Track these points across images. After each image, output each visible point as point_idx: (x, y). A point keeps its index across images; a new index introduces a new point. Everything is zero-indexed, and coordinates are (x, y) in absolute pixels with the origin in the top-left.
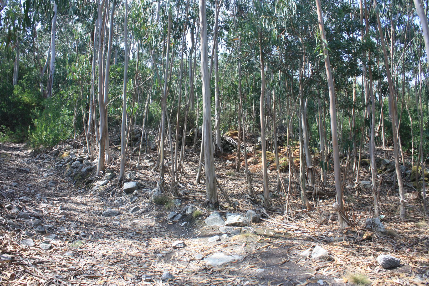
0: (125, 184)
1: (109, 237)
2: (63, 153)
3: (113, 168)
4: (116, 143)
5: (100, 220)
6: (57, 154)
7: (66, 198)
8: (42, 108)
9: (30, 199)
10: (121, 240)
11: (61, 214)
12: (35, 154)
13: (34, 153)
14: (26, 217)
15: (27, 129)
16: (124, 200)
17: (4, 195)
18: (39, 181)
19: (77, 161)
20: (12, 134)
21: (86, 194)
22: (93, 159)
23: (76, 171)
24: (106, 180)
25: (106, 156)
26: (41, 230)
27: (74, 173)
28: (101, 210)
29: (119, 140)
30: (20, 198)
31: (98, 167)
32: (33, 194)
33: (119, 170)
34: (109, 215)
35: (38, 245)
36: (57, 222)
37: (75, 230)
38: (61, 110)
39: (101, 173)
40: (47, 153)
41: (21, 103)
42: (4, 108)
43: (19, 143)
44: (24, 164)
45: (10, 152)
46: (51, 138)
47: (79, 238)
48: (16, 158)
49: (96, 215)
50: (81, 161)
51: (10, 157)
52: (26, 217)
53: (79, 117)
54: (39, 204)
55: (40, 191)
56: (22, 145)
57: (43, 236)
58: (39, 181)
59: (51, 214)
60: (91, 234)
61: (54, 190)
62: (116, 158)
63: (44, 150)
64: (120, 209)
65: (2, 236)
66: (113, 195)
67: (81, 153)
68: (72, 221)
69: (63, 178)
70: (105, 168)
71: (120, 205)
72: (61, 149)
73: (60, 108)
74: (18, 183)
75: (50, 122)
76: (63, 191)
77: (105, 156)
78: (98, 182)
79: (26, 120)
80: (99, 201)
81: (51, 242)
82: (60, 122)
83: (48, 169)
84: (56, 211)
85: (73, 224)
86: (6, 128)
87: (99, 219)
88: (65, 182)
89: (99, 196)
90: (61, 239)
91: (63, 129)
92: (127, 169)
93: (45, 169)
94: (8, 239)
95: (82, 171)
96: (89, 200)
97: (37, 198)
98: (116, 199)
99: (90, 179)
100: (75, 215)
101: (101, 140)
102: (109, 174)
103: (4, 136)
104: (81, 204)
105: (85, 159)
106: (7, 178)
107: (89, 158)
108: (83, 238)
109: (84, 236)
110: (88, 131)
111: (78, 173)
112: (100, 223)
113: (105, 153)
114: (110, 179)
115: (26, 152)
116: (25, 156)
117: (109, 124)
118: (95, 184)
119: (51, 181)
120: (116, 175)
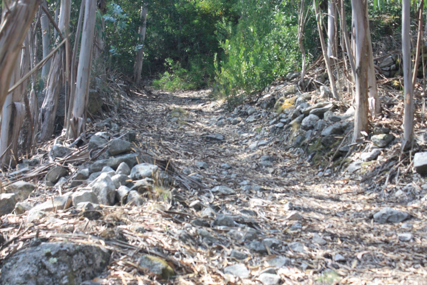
0: (417, 155)
1: (393, 264)
2: (282, 101)
3: (386, 125)
4: (387, 73)
5: (370, 230)
6: (271, 103)
7: (297, 187)
8: (235, 19)
9: (232, 191)
10: (420, 271)
11: (292, 218)
12: (229, 108)
13: (228, 105)
14: (228, 223)
15: (212, 62)
16: (418, 189)
17: (186, 184)
18: (244, 156)
19: (311, 116)
20: (184, 74)
21: (335, 180)
22: (344, 109)
23: (312, 135)
24: (374, 150)
25: (371, 100)
26: (258, 249)
27: (307, 140)
28: (369, 210)
29: (393, 66)
30: (213, 190)
31: (356, 124)
32: (234, 180)
33: (399, 128)
34: (388, 219)
35: (257, 277)
36: (285, 233)
37: (322, 248)
38: (274, 18)
39: (362, 135)
40: (252, 103)
41: (195, 14)
42: (167, 26)
43: (198, 89)
44: (213, 127)
45: (185, 107)
46: (258, 74)
47: (333, 265)
48: (197, 116)
49: (361, 221)
50: (320, 114)
51: (188, 115)
52: (229, 223)
53: (310, 24)
54: (248, 199)
55: (247, 176)
56: (204, 93)
57: (264, 259)
58: (244, 156)
59: (273, 218)
60: (355, 257)
61: (273, 173)
62: (391, 105)
63: (246, 98)
64: (410, 208)
65: (193, 257)
66: (391, 180)
67: (317, 98)
68: (314, 232)
69: (287, 150)
70: (372, 126)
71: (409, 201)
72: (279, 93)
73: (268, 13)
74: (207, 162)
75: (253, 43)
76: (289, 174)
77: (370, 100)
78: (357, 155)
79: (207, 44)
80: (363, 193)
81: (279, 272)
82: (272, 42)
83: (257, 134)
84: (281, 213)
85: (318, 238)
86: (174, 63)
87: (368, 228)
88: (291, 158)
89: (362, 181)
90: (297, 267)
91: (279, 53)
92: (417, 126)
93: (251, 135)
94: (202, 263)
95: (323, 133)
96: (343, 190)
97: (243, 188)
98: (398, 187)
99: (342, 149)
100: (318, 220)
101: (360, 68)
102: (381, 136)
103: (172, 79)
104: (327, 198)
105: (327, 109)
106: (186, 154)
107: (335, 108)
108: (340, 265)
109: (343, 262)
110: (328, 53)
111: (315, 139)
112: (371, 235)
113: (369, 94)
114: (383, 147)
115: (213, 104)
116: (213, 113)
117: (373, 37)
118: (353, 158)
119: (265, 156)
120: (394, 137)
